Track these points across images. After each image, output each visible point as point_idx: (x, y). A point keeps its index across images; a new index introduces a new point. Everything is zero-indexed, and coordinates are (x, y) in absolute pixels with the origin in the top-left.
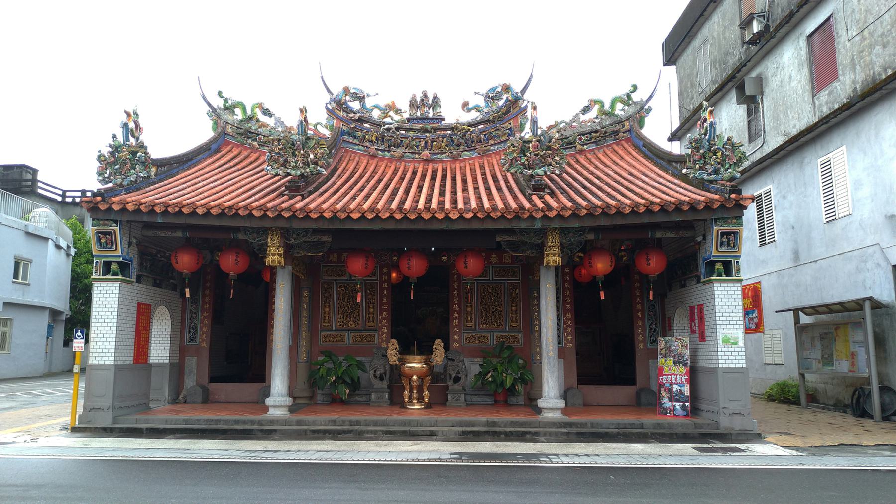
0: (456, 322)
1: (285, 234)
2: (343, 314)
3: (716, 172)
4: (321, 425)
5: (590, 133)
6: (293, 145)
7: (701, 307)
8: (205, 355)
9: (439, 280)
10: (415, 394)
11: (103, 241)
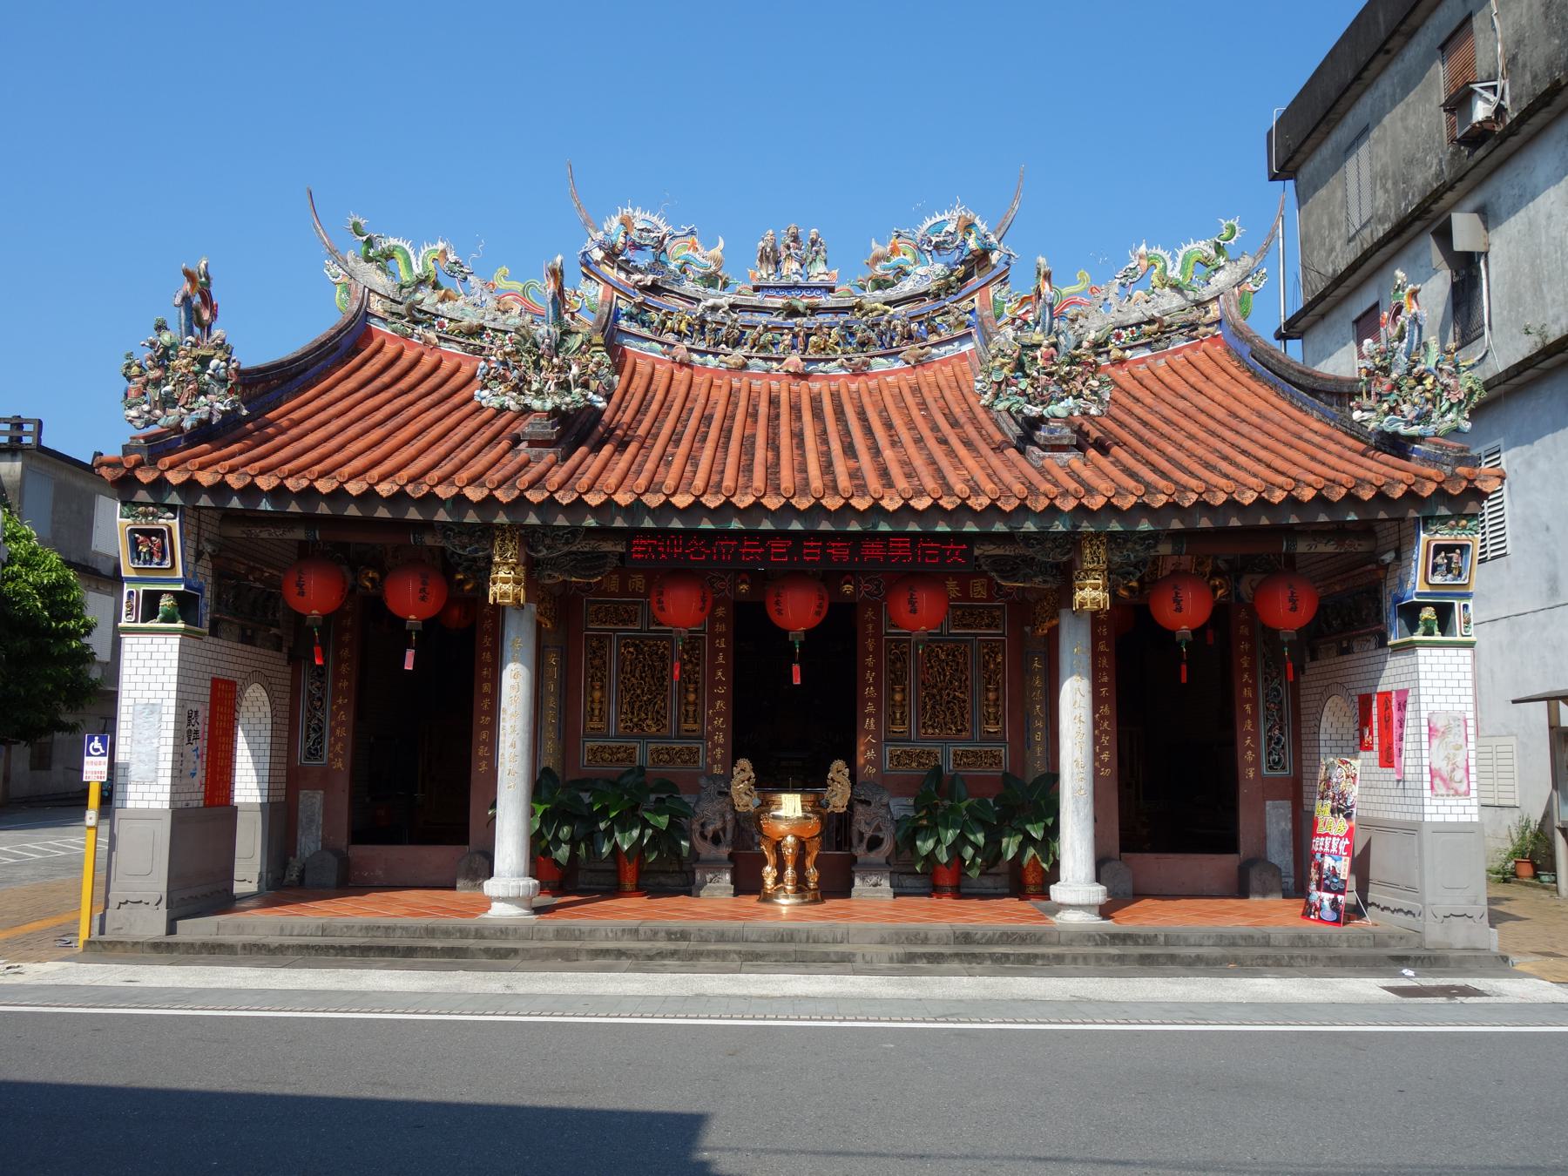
0: (870, 723)
1: (529, 538)
3: (1423, 418)
4: (607, 938)
5: (1138, 325)
6: (536, 345)
8: (343, 784)
9: (838, 637)
10: (789, 872)
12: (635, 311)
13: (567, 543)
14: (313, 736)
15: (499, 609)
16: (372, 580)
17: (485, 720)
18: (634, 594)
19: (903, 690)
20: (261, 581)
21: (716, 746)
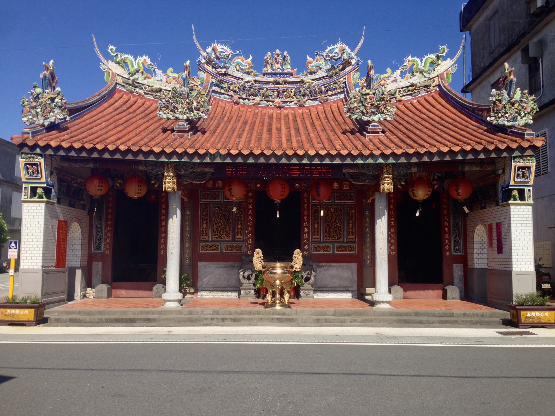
1: (177, 167)
2: (217, 229)
5: (407, 87)
7: (499, 225)
11: (30, 171)
12: (218, 83)
13: (192, 168)
14: (98, 242)
15: (167, 193)
16: (120, 183)
17: (163, 235)
18: (218, 188)
19: (318, 223)
20: (77, 184)
21: (248, 244)
